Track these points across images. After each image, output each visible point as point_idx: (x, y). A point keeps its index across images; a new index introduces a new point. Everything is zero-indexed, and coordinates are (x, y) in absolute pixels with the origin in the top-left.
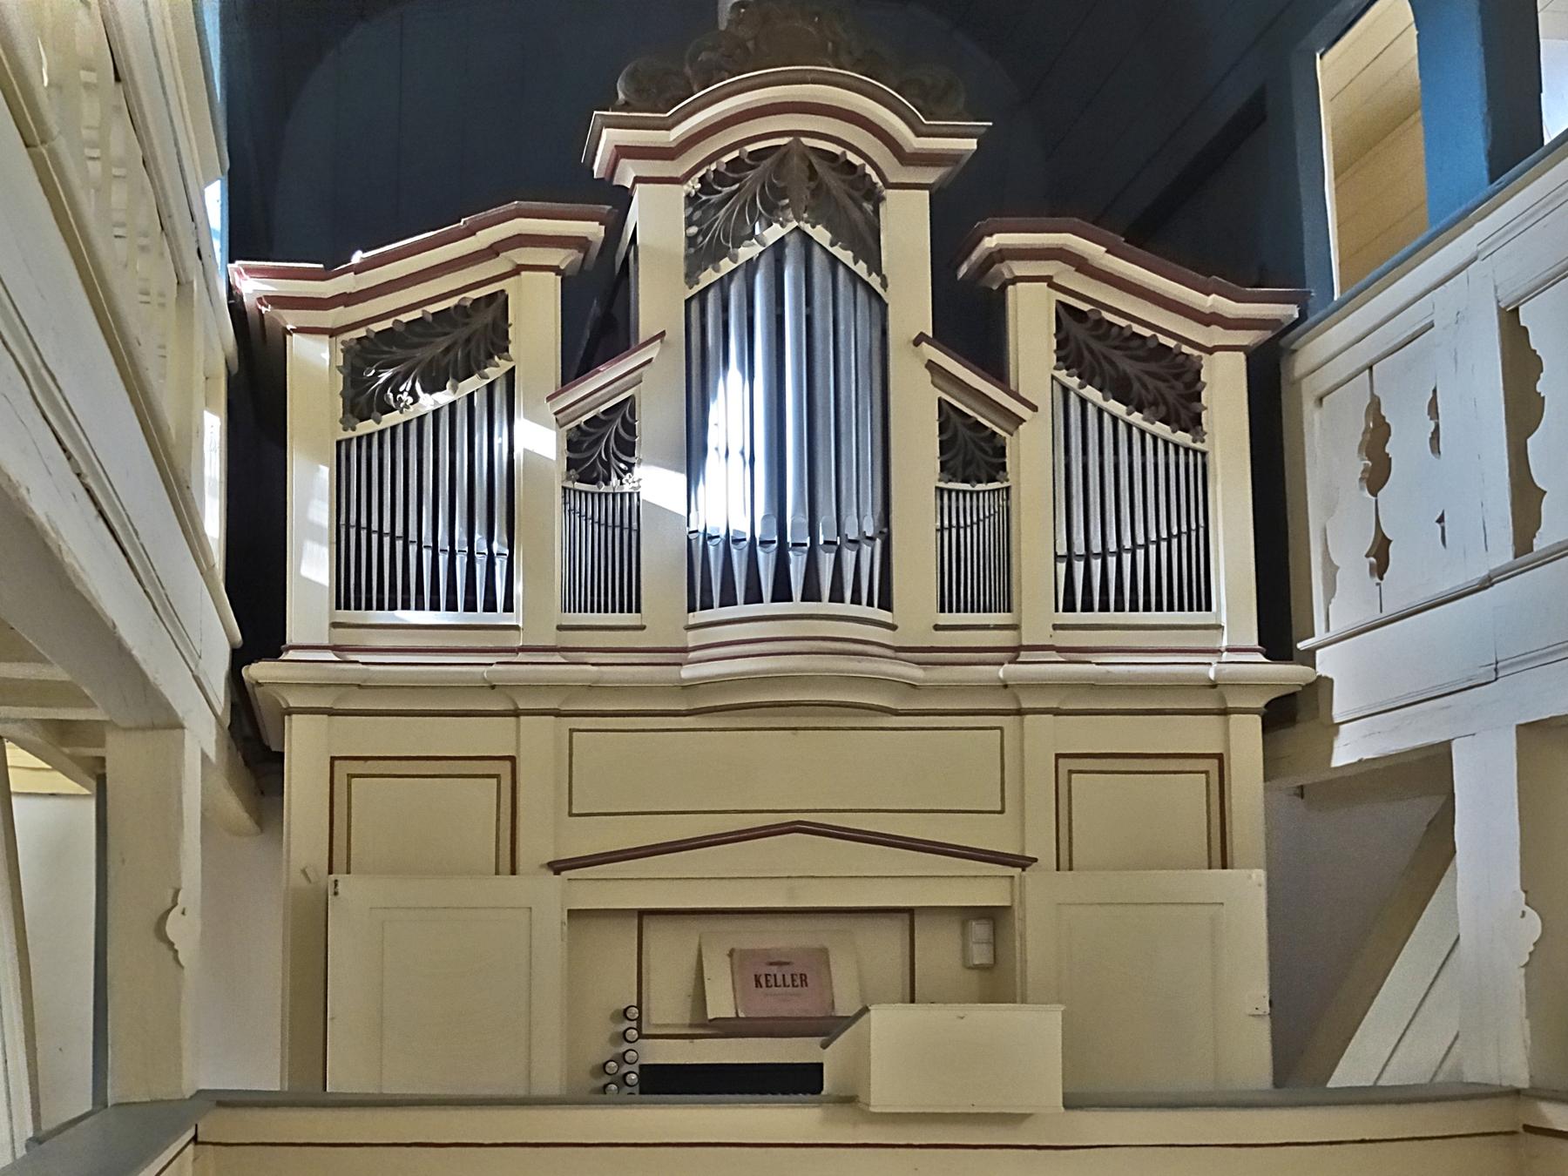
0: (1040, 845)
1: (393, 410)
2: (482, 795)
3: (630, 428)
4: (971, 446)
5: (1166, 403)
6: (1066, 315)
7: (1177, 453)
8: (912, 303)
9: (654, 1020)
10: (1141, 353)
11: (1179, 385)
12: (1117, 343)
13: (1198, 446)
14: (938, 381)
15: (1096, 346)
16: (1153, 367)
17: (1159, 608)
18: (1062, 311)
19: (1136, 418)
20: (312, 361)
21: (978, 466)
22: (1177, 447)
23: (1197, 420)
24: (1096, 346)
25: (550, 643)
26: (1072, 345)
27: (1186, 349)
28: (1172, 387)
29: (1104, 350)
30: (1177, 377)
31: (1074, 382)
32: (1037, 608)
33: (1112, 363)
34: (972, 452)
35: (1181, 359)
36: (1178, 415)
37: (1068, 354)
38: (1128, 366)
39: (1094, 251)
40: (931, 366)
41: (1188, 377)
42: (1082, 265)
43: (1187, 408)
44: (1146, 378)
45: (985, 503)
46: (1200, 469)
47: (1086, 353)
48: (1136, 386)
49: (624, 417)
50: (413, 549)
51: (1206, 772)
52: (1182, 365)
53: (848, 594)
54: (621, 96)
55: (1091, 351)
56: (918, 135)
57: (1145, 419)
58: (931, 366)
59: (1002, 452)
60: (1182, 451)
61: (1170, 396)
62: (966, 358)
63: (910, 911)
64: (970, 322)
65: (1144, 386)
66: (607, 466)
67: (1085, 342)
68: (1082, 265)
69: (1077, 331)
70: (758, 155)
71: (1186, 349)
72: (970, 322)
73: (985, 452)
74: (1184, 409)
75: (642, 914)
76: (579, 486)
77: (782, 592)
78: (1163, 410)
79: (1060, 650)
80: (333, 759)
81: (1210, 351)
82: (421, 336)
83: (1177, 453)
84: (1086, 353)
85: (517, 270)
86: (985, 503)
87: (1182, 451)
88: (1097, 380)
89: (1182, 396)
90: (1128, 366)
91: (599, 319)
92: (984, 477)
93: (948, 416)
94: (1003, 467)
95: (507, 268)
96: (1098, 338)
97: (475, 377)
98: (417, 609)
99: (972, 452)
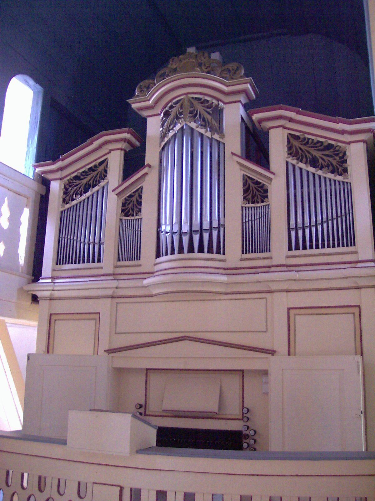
0: (281, 345)
1: (75, 200)
2: (346, 322)
3: (141, 197)
4: (255, 190)
5: (332, 164)
6: (291, 138)
7: (335, 184)
8: (233, 141)
9: (151, 409)
10: (322, 148)
11: (337, 158)
12: (312, 145)
13: (346, 180)
14: (241, 168)
15: (303, 147)
16: (327, 152)
17: (343, 246)
18: (290, 137)
19: (320, 172)
20: (56, 187)
21: (258, 198)
22: (339, 182)
23: (345, 170)
24: (303, 147)
25: (284, 263)
26: (294, 148)
27: (340, 144)
28: (335, 159)
29: (306, 148)
30: (337, 155)
31: (294, 162)
32: (279, 248)
33: (309, 153)
34: (255, 192)
35: (337, 148)
36: (338, 169)
37: (292, 151)
38: (318, 154)
39: (292, 115)
40: (238, 163)
41: (341, 155)
42: (291, 120)
43: (341, 166)
44: (324, 157)
45: (262, 211)
46: (348, 189)
47: (300, 151)
48: (320, 160)
49: (139, 194)
50: (75, 242)
51: (354, 313)
52: (338, 150)
53: (206, 249)
54: (136, 94)
55: (301, 149)
56: (149, 100)
57: (323, 173)
58: (238, 163)
59: (266, 191)
60: (341, 184)
61: (334, 163)
62: (136, 171)
63: (242, 372)
64: (256, 147)
65: (323, 159)
66: (133, 210)
67: (298, 147)
68: (291, 120)
69: (296, 143)
70: (176, 103)
71: (340, 144)
72: (256, 147)
73: (261, 192)
74: (340, 166)
75: (147, 370)
76: (126, 218)
77: (181, 251)
78: (331, 168)
79: (225, 269)
80: (289, 309)
81: (349, 143)
82: (85, 175)
83: (335, 184)
84: (300, 151)
85: (110, 152)
86: (262, 211)
87: (341, 184)
88: (304, 160)
89: (338, 162)
90: (318, 154)
91: (134, 162)
92: (260, 200)
93: (247, 181)
94: (267, 197)
95: (108, 151)
96: (305, 144)
97: (97, 186)
98: (342, 247)
99: (255, 192)
